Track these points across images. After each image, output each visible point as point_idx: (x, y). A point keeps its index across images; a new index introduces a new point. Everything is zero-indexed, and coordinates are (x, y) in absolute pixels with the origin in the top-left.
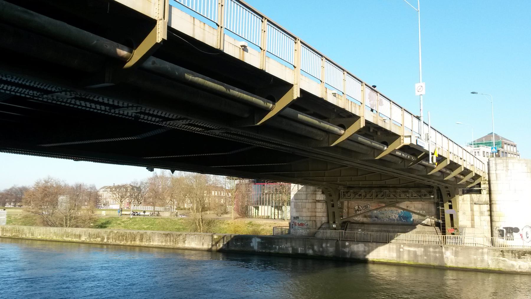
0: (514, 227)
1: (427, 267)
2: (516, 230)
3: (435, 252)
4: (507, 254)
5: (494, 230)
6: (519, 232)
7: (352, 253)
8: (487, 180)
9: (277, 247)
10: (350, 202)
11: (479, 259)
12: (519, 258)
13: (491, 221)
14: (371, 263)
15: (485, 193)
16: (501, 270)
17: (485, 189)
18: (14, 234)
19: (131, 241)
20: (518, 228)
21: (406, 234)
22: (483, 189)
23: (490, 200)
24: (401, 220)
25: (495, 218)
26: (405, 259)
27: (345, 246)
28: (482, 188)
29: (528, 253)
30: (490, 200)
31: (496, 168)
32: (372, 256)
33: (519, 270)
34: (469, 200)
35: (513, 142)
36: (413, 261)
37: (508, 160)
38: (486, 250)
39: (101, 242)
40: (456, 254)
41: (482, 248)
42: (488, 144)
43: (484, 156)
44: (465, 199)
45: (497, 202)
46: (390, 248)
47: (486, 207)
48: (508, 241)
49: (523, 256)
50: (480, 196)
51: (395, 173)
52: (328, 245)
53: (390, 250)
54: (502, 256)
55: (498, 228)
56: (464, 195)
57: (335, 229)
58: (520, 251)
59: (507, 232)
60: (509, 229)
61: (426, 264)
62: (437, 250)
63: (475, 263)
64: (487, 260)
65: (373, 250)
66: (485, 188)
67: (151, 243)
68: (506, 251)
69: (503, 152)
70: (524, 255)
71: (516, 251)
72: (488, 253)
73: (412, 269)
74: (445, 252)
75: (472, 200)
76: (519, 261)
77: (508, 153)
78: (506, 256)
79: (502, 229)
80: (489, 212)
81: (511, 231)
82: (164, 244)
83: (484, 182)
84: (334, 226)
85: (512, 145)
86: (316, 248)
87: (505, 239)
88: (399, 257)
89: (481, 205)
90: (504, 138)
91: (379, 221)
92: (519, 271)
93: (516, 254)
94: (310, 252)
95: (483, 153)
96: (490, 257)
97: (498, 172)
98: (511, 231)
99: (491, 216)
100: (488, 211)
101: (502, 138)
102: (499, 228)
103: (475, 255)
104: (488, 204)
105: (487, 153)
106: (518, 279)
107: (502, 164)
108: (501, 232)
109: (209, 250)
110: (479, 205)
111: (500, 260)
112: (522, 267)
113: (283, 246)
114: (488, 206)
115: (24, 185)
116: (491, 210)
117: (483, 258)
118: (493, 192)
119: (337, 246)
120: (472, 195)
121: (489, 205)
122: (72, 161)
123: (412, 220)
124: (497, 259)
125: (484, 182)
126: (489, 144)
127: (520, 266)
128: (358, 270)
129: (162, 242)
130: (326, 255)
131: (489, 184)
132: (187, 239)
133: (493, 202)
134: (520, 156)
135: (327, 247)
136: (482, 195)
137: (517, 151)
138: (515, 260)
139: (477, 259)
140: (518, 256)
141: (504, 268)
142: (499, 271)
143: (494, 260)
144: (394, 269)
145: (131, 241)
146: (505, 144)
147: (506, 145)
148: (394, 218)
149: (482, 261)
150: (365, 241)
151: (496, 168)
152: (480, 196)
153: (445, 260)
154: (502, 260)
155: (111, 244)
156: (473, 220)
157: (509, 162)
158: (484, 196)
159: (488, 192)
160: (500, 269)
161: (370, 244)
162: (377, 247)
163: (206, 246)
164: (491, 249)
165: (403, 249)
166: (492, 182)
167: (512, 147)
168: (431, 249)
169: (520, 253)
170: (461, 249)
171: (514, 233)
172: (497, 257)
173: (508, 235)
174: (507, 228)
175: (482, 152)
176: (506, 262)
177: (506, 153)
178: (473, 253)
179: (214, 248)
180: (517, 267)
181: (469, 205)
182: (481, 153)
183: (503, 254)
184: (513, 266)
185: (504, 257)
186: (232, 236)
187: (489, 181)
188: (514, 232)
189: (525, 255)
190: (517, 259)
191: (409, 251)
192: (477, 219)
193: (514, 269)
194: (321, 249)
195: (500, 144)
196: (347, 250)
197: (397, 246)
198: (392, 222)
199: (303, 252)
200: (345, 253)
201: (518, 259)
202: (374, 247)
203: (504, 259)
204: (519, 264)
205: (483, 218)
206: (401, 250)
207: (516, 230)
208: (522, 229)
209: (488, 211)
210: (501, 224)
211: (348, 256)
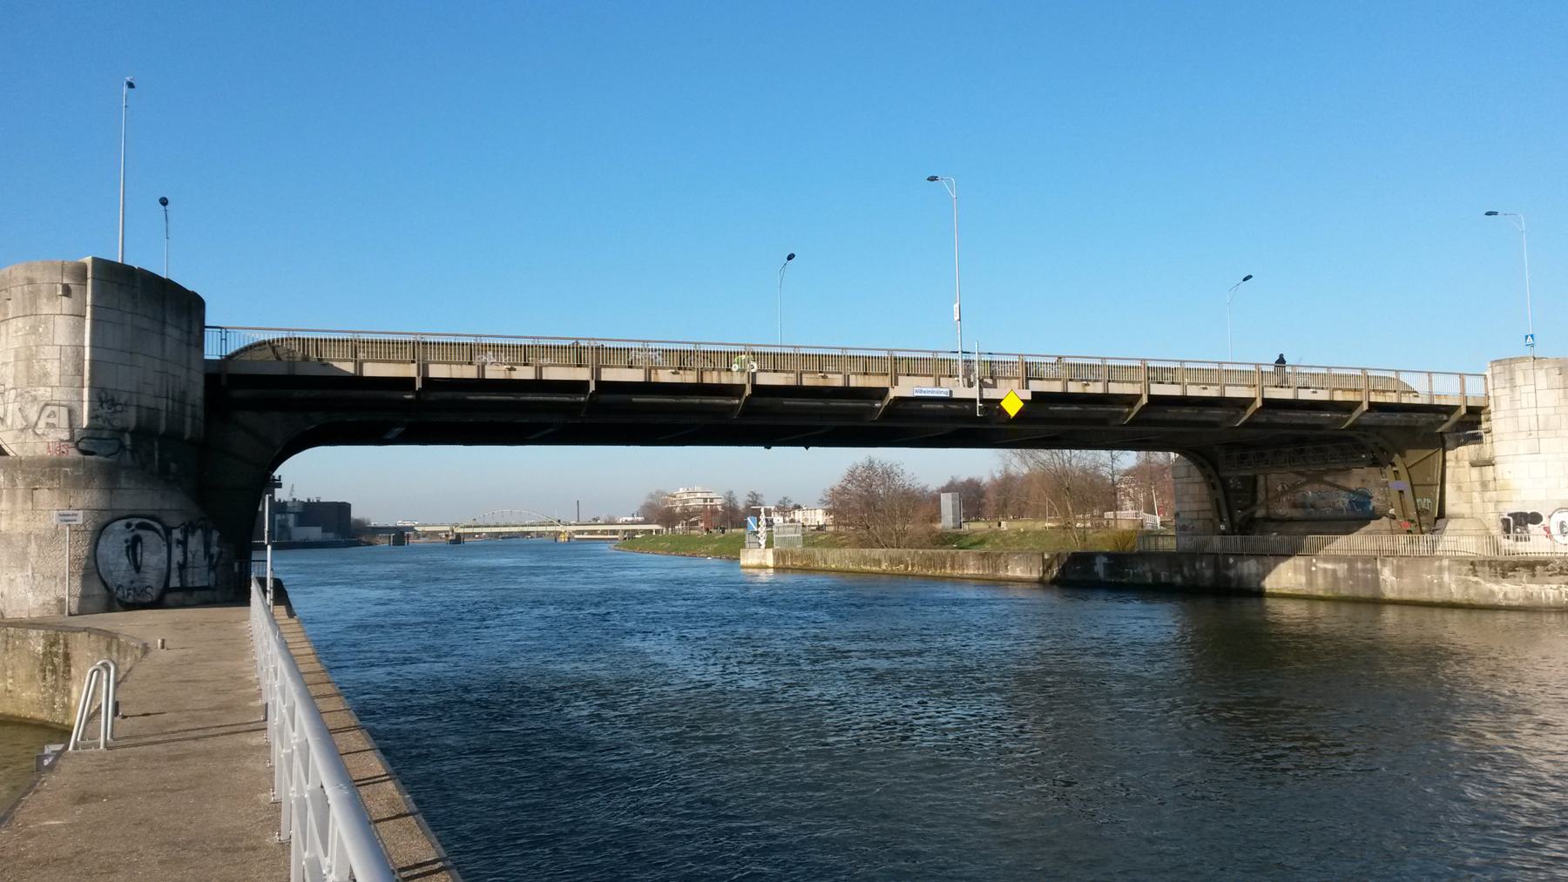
0: (1529, 512)
1: (1355, 601)
2: (1535, 518)
3: (1365, 570)
6: (1542, 523)
7: (1240, 578)
9: (1131, 572)
10: (1268, 477)
11: (1435, 581)
12: (1504, 576)
14: (1268, 597)
16: (1472, 602)
18: (805, 562)
19: (941, 569)
21: (1351, 536)
24: (1353, 510)
26: (1321, 587)
27: (1228, 567)
29: (1523, 566)
32: (1270, 584)
33: (1504, 603)
36: (1333, 589)
37: (1513, 365)
38: (1446, 563)
39: (905, 572)
40: (1398, 572)
44: (1460, 457)
46: (1295, 565)
48: (1519, 543)
49: (1511, 571)
50: (1480, 449)
52: (1204, 565)
53: (1296, 570)
56: (1460, 448)
57: (1223, 533)
58: (1505, 562)
59: (1518, 524)
61: (1352, 595)
62: (1369, 566)
63: (1430, 590)
65: (1270, 571)
67: (966, 572)
70: (1514, 570)
72: (1449, 569)
74: (1381, 569)
78: (1479, 574)
79: (1506, 517)
81: (1523, 522)
82: (981, 572)
84: (1222, 527)
86: (1186, 570)
88: (1310, 582)
91: (1318, 515)
92: (1504, 604)
93: (1498, 569)
94: (1178, 579)
96: (1454, 577)
98: (1523, 522)
103: (1430, 572)
109: (1041, 581)
112: (1510, 595)
113: (1139, 570)
115: (972, 477)
117: (1442, 578)
119: (1216, 567)
122: (762, 449)
123: (1371, 508)
127: (1505, 594)
128: (1249, 606)
129: (978, 569)
130: (1201, 584)
132: (1010, 561)
135: (1202, 568)
136: (1484, 446)
138: (1497, 582)
142: (1526, 603)
143: (1460, 583)
144: (1304, 605)
145: (941, 569)
148: (1341, 505)
149: (1441, 585)
150: (1259, 555)
152: (1480, 449)
153: (1382, 586)
155: (918, 574)
161: (1266, 560)
162: (1276, 565)
163: (1035, 575)
165: (1316, 566)
168: (1360, 565)
169: (1506, 565)
170: (1407, 562)
171: (1529, 525)
173: (1518, 530)
174: (1514, 515)
178: (1425, 569)
179: (1047, 577)
180: (1501, 596)
184: (1492, 593)
185: (1476, 576)
186: (1070, 554)
189: (1516, 571)
191: (1325, 570)
193: (1495, 601)
194: (1194, 573)
196: (1232, 573)
197: (1306, 562)
198: (1340, 515)
199: (1169, 581)
200: (1229, 579)
202: (1272, 564)
203: (1476, 579)
204: (1504, 589)
206: (1313, 569)
208: (1550, 517)
211: (1233, 585)
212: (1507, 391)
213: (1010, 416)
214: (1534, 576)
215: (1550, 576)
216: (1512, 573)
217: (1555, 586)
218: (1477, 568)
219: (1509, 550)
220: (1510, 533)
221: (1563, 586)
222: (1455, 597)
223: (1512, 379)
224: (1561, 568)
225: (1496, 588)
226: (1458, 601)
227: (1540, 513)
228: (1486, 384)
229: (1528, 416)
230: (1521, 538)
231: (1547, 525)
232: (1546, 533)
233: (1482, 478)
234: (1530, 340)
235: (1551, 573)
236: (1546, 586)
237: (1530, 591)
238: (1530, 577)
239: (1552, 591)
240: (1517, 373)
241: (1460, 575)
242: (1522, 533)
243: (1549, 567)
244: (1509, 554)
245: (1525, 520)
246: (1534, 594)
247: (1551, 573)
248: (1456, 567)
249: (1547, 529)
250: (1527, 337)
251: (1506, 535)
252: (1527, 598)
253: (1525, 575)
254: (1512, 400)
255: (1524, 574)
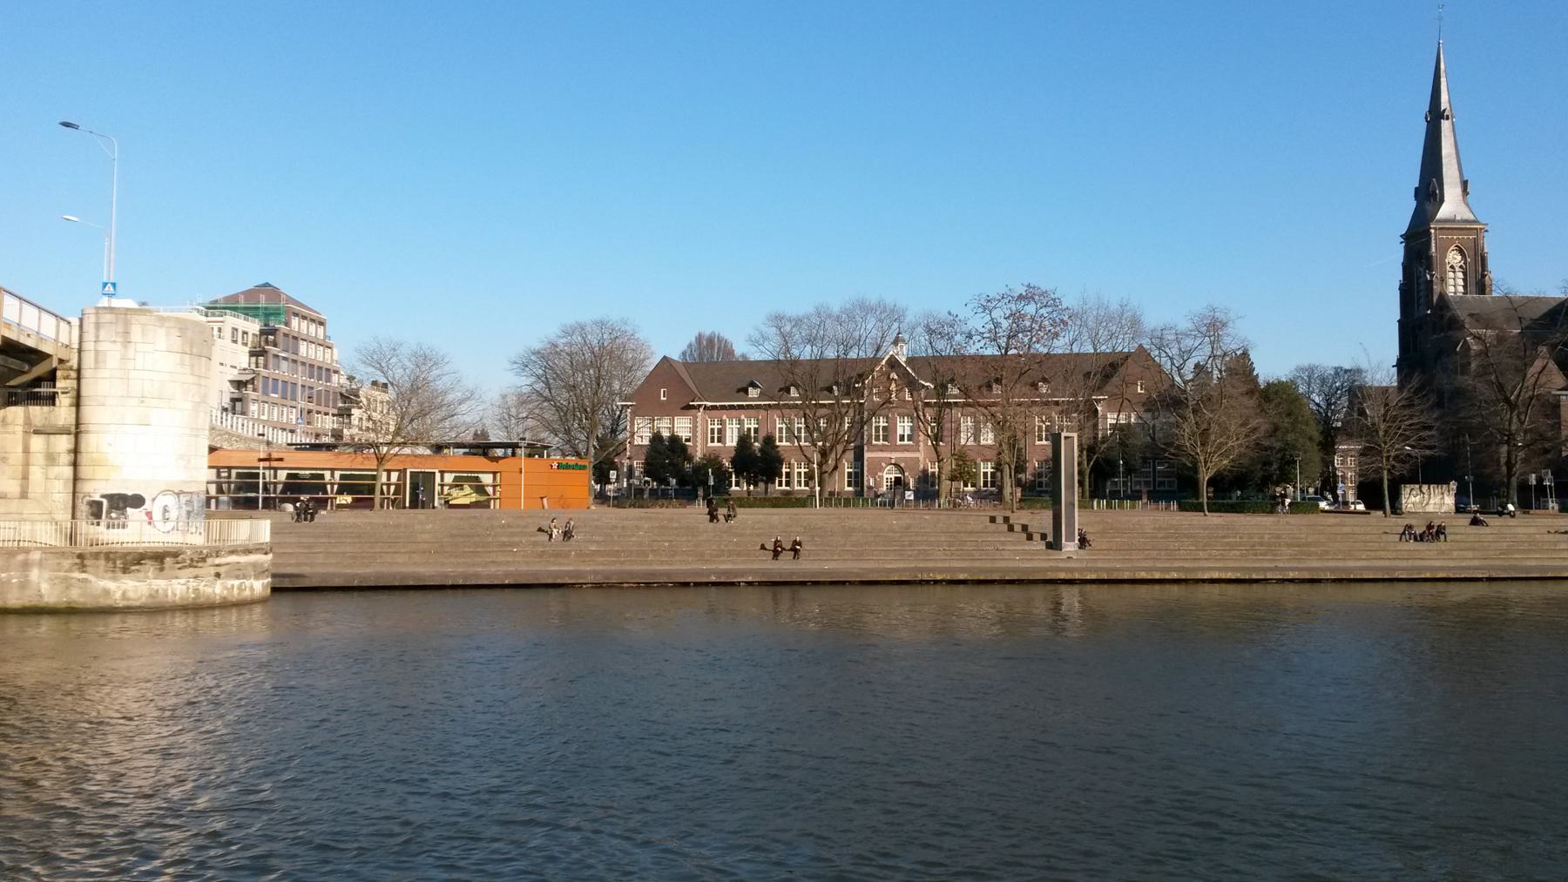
0: (130, 494)
2: (137, 501)
4: (94, 561)
5: (79, 502)
6: (144, 507)
8: (75, 367)
12: (125, 570)
13: (76, 479)
15: (64, 401)
16: (75, 606)
17: (66, 393)
20: (141, 496)
22: (59, 391)
23: (78, 424)
25: (85, 471)
28: (59, 388)
30: (78, 424)
31: (97, 336)
33: (121, 604)
34: (21, 421)
35: (318, 313)
37: (129, 316)
38: (36, 556)
41: (27, 551)
42: (251, 313)
43: (235, 342)
44: (9, 419)
45: (91, 428)
47: (63, 443)
48: (111, 530)
49: (135, 564)
50: (50, 412)
51: (1266, 580)
54: (79, 568)
55: (88, 498)
56: (8, 408)
59: (112, 507)
60: (118, 499)
64: (37, 581)
66: (67, 388)
68: (91, 555)
69: (286, 335)
70: (139, 564)
71: (117, 555)
73: (767, 593)
75: (28, 421)
76: (123, 581)
77: (302, 339)
79: (97, 498)
80: (73, 455)
81: (121, 505)
83: (65, 373)
85: (313, 321)
87: (102, 524)
89: (52, 436)
90: (294, 300)
92: (121, 605)
93: (118, 562)
95: (233, 332)
97: (103, 346)
98: (121, 505)
99: (75, 465)
100: (69, 452)
101: (290, 300)
102: (90, 496)
104: (69, 434)
105: (245, 335)
106: (115, 622)
107: (113, 327)
108: (95, 509)
110: (46, 436)
111: (73, 580)
112: (131, 594)
114: (72, 437)
116: (76, 451)
118: (84, 401)
120: (31, 408)
121: (72, 436)
124: (66, 579)
125: (65, 373)
126: (250, 312)
127: (124, 594)
131: (79, 379)
133: (83, 428)
134: (335, 350)
136: (56, 409)
137: (325, 336)
138: (114, 579)
139: (9, 581)
140: (122, 566)
141: (82, 600)
142: (150, 602)
146: (296, 315)
147: (297, 318)
149: (24, 585)
151: (97, 336)
152: (50, 412)
154: (79, 580)
156: (25, 477)
157: (133, 321)
158: (63, 412)
159: (74, 401)
160: (70, 603)
164: (52, 553)
166: (86, 373)
167: (314, 325)
169: (129, 558)
171: (128, 509)
172: (66, 572)
173: (113, 515)
174: (110, 497)
175: (230, 331)
176: (88, 585)
177: (295, 338)
180: (118, 595)
181: (20, 435)
182: (227, 333)
183: (83, 562)
184: (107, 592)
185: (83, 572)
187: (79, 371)
188: (128, 509)
189: (142, 564)
190: (120, 574)
192: (36, 473)
195: (280, 314)
201: (122, 575)
203: (84, 575)
204: (123, 587)
205: (56, 470)
207: (137, 501)
208: (154, 500)
209: (69, 452)
210: (96, 488)
212: (118, 346)
213: (1355, 391)
214: (162, 569)
215: (179, 569)
216: (137, 567)
217: (183, 581)
218: (86, 562)
219: (98, 540)
220: (101, 518)
221: (191, 580)
222: (46, 599)
223: (127, 333)
224: (192, 560)
225: (111, 585)
226: (52, 606)
227: (143, 495)
228: (70, 333)
229: (143, 379)
230: (119, 525)
231: (149, 510)
232: (146, 518)
233: (48, 448)
234: (109, 288)
235: (179, 566)
236: (174, 581)
237: (155, 588)
238: (157, 571)
239: (179, 586)
240: (133, 326)
241: (59, 571)
242: (117, 518)
243: (179, 559)
244: (98, 545)
245: (124, 502)
246: (160, 591)
247: (179, 566)
248: (52, 561)
249: (149, 514)
250: (105, 285)
251: (95, 521)
252: (151, 596)
253: (152, 569)
254: (124, 358)
255: (150, 568)
